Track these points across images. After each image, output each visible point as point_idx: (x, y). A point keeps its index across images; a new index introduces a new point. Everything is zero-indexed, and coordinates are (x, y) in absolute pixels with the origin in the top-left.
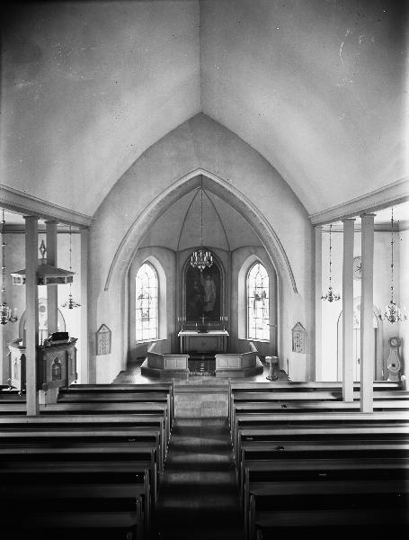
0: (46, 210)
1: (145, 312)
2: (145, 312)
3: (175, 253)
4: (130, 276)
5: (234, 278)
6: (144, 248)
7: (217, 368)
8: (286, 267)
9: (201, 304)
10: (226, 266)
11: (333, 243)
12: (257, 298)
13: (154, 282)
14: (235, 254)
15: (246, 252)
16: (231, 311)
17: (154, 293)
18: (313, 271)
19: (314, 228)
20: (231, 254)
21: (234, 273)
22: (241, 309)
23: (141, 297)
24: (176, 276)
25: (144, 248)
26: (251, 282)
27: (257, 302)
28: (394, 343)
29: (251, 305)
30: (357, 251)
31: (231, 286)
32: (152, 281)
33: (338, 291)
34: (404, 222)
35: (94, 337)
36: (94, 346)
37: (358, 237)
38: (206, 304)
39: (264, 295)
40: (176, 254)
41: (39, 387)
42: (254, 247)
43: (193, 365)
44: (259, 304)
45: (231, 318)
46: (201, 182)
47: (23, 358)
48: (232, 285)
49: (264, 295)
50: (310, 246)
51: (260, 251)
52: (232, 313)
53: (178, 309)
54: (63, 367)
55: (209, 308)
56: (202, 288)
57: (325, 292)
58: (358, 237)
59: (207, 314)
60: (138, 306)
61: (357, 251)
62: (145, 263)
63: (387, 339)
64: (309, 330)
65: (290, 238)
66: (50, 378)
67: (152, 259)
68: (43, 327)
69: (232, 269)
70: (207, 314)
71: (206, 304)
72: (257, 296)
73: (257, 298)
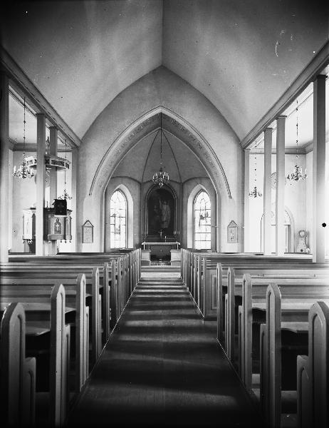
0: (53, 115)
1: (117, 227)
2: (117, 227)
3: (139, 182)
4: (106, 196)
5: (184, 203)
6: (116, 177)
7: (172, 259)
8: (222, 177)
9: (160, 223)
10: (178, 194)
11: (256, 163)
12: (202, 218)
13: (124, 207)
14: (185, 186)
15: (193, 183)
16: (182, 228)
17: (124, 214)
18: (243, 183)
19: (243, 148)
20: (182, 185)
21: (185, 200)
22: (189, 226)
23: (114, 216)
24: (140, 214)
25: (116, 177)
26: (197, 206)
27: (202, 221)
28: (302, 234)
29: (197, 224)
30: (274, 169)
31: (182, 206)
32: (123, 204)
33: (260, 190)
34: (327, 262)
35: (81, 228)
36: (81, 236)
37: (274, 157)
38: (163, 223)
39: (207, 216)
40: (141, 184)
41: (45, 238)
42: (200, 178)
43: (154, 258)
44: (203, 222)
45: (182, 233)
46: (161, 121)
47: (34, 216)
48: (183, 208)
49: (207, 216)
50: (241, 189)
51: (205, 182)
52: (182, 228)
53: (142, 226)
54: (62, 226)
55: (165, 226)
56: (160, 211)
57: (252, 190)
58: (274, 157)
59: (164, 230)
60: (112, 222)
61: (274, 169)
62: (117, 190)
63: (297, 232)
64: (239, 225)
65: (223, 152)
66: (53, 232)
67: (122, 186)
68: (48, 199)
69: (183, 197)
70: (164, 230)
71: (163, 223)
72: (201, 216)
73: (202, 218)
